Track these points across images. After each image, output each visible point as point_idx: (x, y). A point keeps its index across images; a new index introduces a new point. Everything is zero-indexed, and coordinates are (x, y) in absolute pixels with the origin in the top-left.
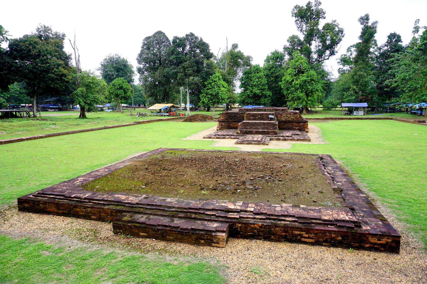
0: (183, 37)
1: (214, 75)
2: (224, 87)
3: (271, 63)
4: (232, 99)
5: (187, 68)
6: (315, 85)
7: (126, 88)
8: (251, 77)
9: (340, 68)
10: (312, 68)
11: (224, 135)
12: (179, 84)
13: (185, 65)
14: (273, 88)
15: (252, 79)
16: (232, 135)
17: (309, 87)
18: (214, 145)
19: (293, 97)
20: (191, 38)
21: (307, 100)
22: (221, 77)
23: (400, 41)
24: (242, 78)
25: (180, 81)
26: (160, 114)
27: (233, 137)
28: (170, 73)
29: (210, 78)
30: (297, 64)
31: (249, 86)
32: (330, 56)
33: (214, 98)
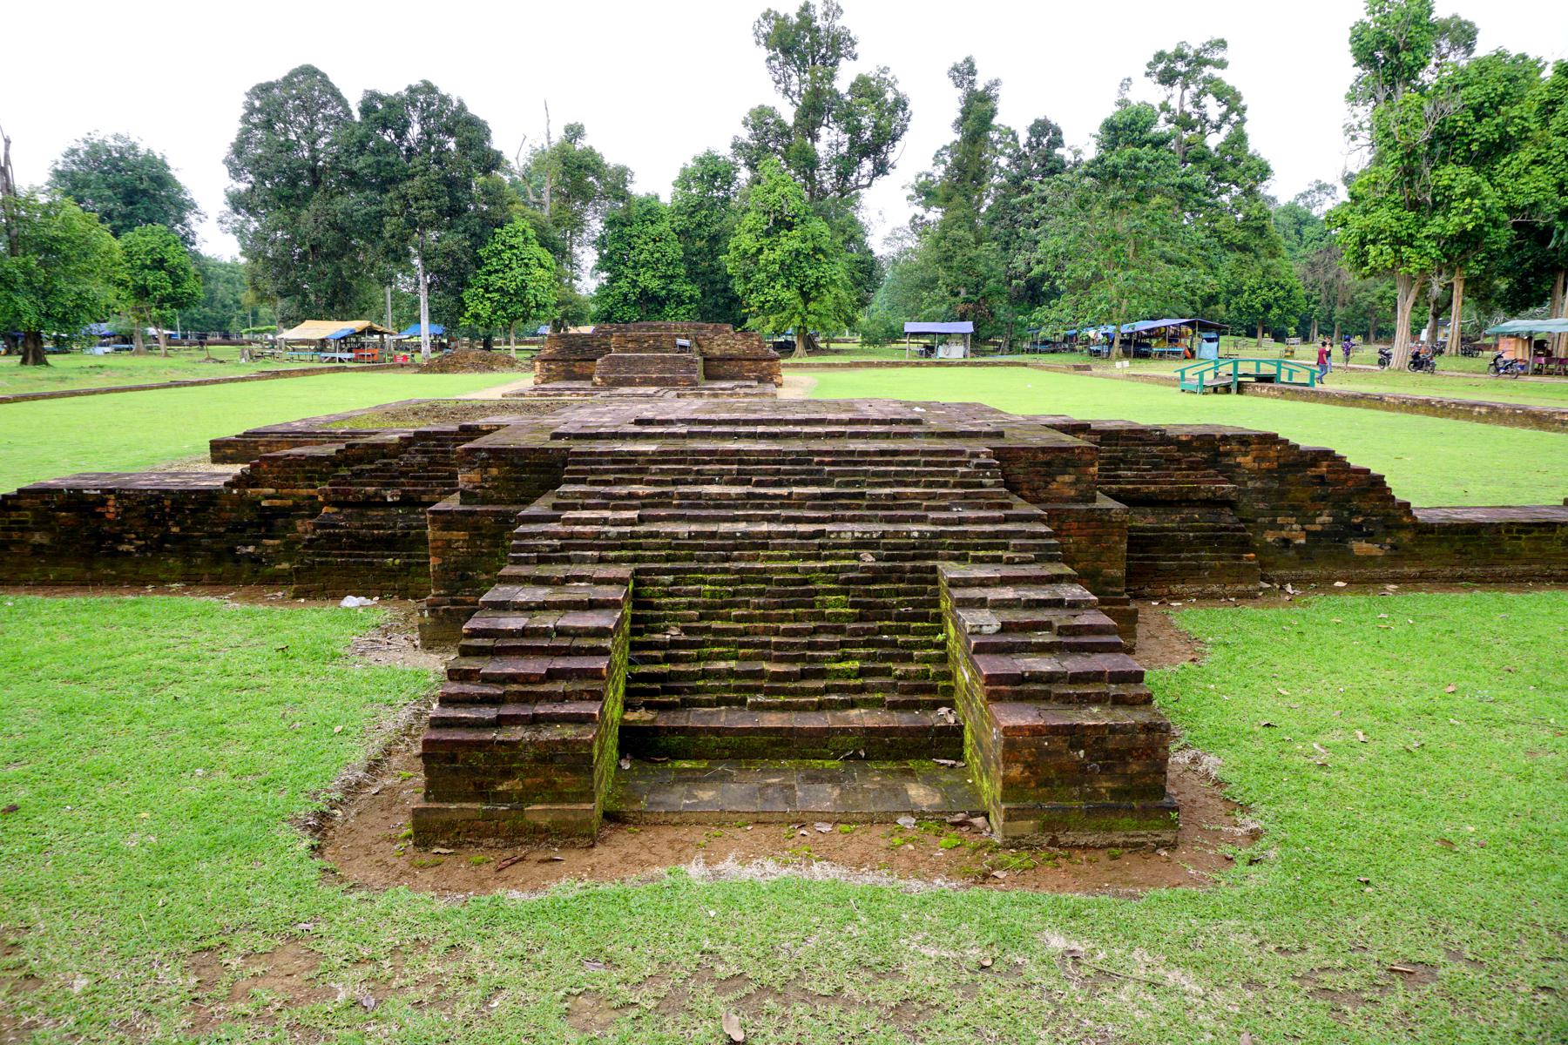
0: (397, 94)
1: (508, 227)
2: (542, 266)
3: (694, 191)
4: (570, 308)
5: (416, 200)
7: (179, 265)
8: (631, 236)
9: (916, 216)
10: (818, 212)
11: (558, 389)
12: (391, 255)
13: (410, 191)
14: (704, 274)
16: (579, 389)
19: (763, 303)
20: (425, 100)
21: (805, 313)
22: (531, 233)
23: (1058, 143)
24: (603, 237)
25: (394, 243)
26: (323, 355)
28: (358, 216)
30: (771, 198)
31: (625, 264)
32: (874, 176)
33: (511, 300)
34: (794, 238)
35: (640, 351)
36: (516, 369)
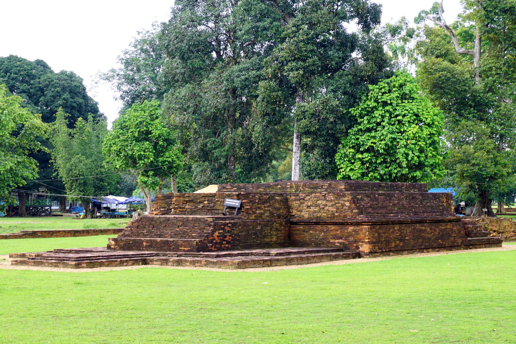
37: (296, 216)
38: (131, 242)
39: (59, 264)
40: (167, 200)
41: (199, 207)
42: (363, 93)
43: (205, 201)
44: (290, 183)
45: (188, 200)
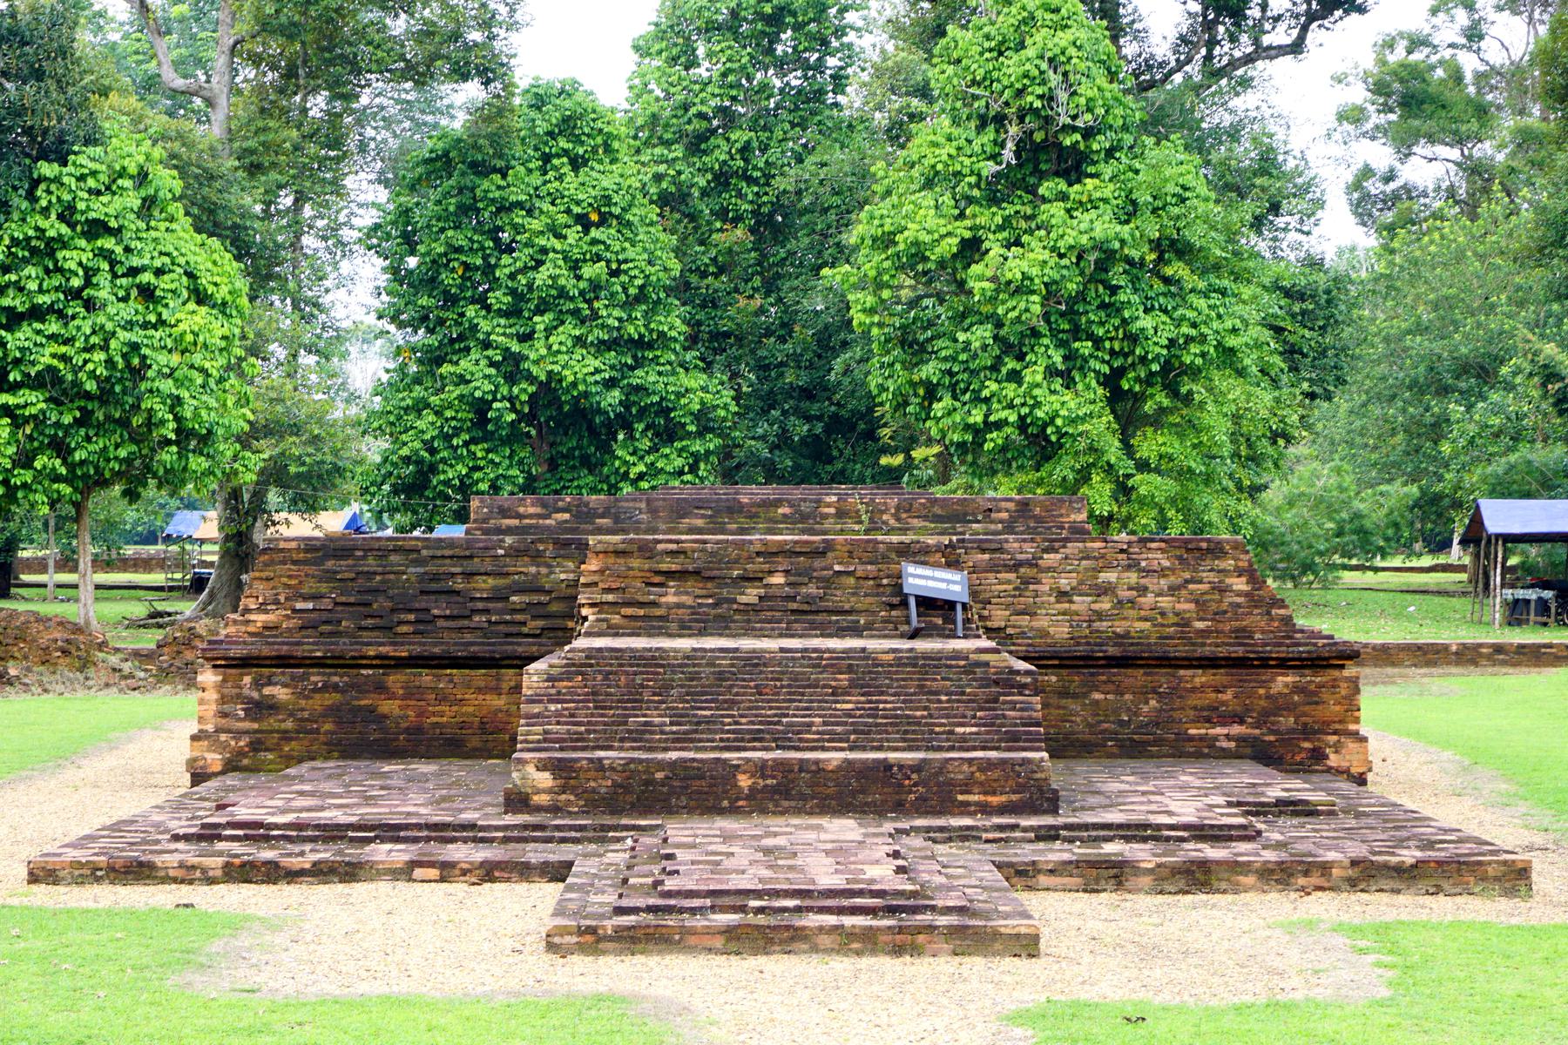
1: (85, 159)
2: (201, 297)
3: (702, 72)
4: (294, 445)
6: (1202, 303)
8: (504, 208)
9: (1367, 172)
11: (332, 833)
15: (518, 229)
16: (442, 832)
17: (1146, 322)
18: (245, 976)
19: (979, 432)
21: (1125, 466)
22: (167, 181)
27: (459, 852)
29: (35, 183)
30: (1013, 67)
31: (481, 301)
32: (1312, 17)
33: (84, 420)
34: (1093, 204)
35: (721, 625)
36: (98, 676)
37: (1010, 631)
38: (659, 775)
39: (921, 938)
40: (330, 564)
41: (743, 599)
42: (15, 188)
43: (771, 573)
44: (834, 499)
45: (674, 567)
